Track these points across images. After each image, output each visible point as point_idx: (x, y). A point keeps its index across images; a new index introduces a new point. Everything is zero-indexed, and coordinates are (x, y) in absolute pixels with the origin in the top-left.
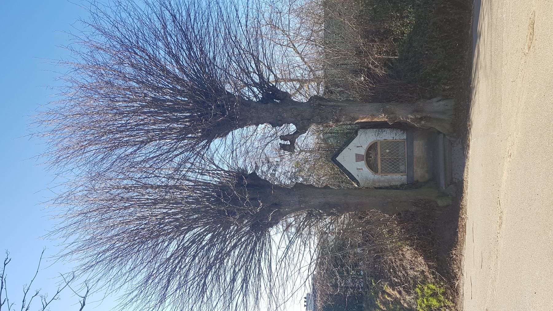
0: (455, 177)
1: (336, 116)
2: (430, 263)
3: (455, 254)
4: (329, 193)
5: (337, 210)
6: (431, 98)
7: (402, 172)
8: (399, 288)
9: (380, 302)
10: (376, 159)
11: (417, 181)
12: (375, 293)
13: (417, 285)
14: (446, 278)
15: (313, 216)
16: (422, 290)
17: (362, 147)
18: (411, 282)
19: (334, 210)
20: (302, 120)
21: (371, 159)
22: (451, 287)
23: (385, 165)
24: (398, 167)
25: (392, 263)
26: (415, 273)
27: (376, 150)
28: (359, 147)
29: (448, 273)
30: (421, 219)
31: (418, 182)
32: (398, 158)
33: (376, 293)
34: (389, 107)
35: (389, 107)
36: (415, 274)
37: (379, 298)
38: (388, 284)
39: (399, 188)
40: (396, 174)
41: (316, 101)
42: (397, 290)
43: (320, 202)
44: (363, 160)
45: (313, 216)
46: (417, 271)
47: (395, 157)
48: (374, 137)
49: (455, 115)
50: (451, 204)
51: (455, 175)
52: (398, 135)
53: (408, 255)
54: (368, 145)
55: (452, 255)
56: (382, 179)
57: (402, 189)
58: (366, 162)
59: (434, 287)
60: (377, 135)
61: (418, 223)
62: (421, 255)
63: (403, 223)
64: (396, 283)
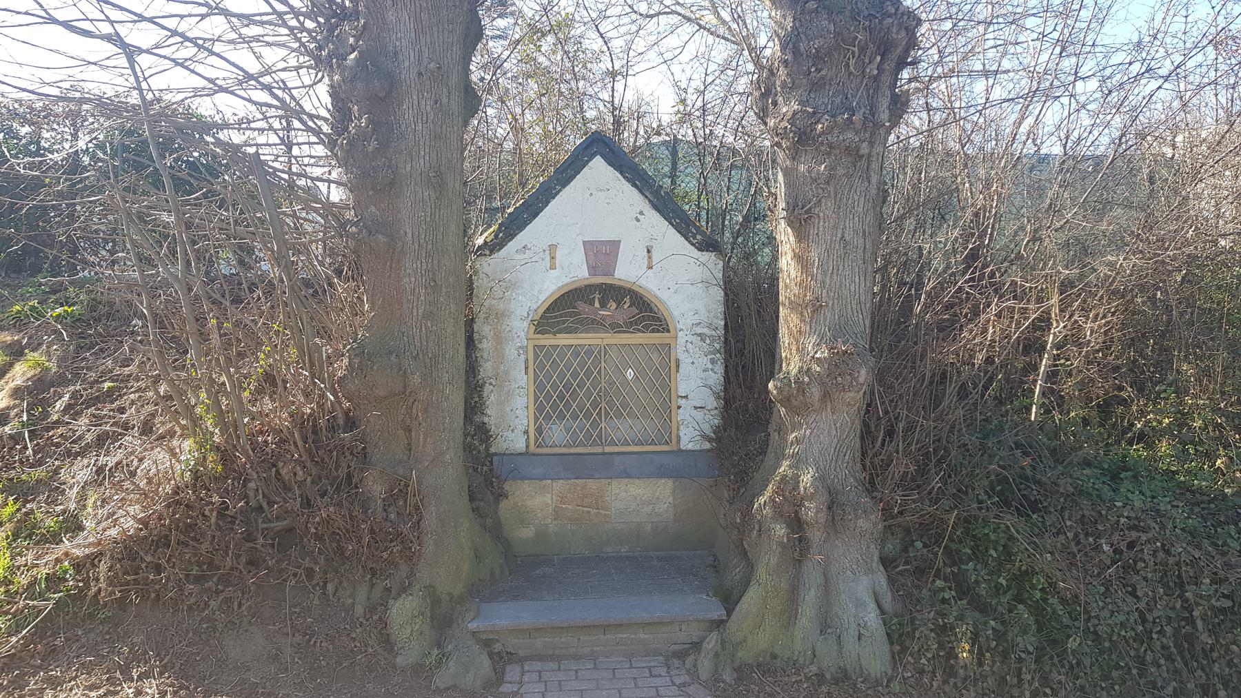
0: (526, 678)
1: (828, 131)
2: (103, 567)
4: (445, 100)
5: (363, 136)
6: (886, 562)
7: (539, 431)
8: (19, 415)
10: (595, 325)
11: (501, 495)
13: (16, 500)
14: (26, 645)
17: (650, 267)
18: (39, 473)
21: (597, 305)
24: (561, 417)
26: (75, 490)
27: (632, 325)
28: (650, 258)
29: (52, 654)
32: (599, 414)
34: (862, 380)
35: (862, 380)
36: (71, 488)
38: (50, 369)
39: (471, 421)
40: (532, 407)
41: (906, 28)
42: (15, 406)
43: (396, 54)
44: (593, 270)
45: (331, 29)
46: (82, 499)
47: (603, 405)
48: (691, 319)
49: (820, 676)
50: (399, 660)
51: (535, 676)
52: (699, 415)
53: (157, 461)
54: (659, 293)
55: (140, 678)
56: (511, 351)
57: (466, 435)
58: (582, 284)
60: (699, 330)
64: (47, 404)
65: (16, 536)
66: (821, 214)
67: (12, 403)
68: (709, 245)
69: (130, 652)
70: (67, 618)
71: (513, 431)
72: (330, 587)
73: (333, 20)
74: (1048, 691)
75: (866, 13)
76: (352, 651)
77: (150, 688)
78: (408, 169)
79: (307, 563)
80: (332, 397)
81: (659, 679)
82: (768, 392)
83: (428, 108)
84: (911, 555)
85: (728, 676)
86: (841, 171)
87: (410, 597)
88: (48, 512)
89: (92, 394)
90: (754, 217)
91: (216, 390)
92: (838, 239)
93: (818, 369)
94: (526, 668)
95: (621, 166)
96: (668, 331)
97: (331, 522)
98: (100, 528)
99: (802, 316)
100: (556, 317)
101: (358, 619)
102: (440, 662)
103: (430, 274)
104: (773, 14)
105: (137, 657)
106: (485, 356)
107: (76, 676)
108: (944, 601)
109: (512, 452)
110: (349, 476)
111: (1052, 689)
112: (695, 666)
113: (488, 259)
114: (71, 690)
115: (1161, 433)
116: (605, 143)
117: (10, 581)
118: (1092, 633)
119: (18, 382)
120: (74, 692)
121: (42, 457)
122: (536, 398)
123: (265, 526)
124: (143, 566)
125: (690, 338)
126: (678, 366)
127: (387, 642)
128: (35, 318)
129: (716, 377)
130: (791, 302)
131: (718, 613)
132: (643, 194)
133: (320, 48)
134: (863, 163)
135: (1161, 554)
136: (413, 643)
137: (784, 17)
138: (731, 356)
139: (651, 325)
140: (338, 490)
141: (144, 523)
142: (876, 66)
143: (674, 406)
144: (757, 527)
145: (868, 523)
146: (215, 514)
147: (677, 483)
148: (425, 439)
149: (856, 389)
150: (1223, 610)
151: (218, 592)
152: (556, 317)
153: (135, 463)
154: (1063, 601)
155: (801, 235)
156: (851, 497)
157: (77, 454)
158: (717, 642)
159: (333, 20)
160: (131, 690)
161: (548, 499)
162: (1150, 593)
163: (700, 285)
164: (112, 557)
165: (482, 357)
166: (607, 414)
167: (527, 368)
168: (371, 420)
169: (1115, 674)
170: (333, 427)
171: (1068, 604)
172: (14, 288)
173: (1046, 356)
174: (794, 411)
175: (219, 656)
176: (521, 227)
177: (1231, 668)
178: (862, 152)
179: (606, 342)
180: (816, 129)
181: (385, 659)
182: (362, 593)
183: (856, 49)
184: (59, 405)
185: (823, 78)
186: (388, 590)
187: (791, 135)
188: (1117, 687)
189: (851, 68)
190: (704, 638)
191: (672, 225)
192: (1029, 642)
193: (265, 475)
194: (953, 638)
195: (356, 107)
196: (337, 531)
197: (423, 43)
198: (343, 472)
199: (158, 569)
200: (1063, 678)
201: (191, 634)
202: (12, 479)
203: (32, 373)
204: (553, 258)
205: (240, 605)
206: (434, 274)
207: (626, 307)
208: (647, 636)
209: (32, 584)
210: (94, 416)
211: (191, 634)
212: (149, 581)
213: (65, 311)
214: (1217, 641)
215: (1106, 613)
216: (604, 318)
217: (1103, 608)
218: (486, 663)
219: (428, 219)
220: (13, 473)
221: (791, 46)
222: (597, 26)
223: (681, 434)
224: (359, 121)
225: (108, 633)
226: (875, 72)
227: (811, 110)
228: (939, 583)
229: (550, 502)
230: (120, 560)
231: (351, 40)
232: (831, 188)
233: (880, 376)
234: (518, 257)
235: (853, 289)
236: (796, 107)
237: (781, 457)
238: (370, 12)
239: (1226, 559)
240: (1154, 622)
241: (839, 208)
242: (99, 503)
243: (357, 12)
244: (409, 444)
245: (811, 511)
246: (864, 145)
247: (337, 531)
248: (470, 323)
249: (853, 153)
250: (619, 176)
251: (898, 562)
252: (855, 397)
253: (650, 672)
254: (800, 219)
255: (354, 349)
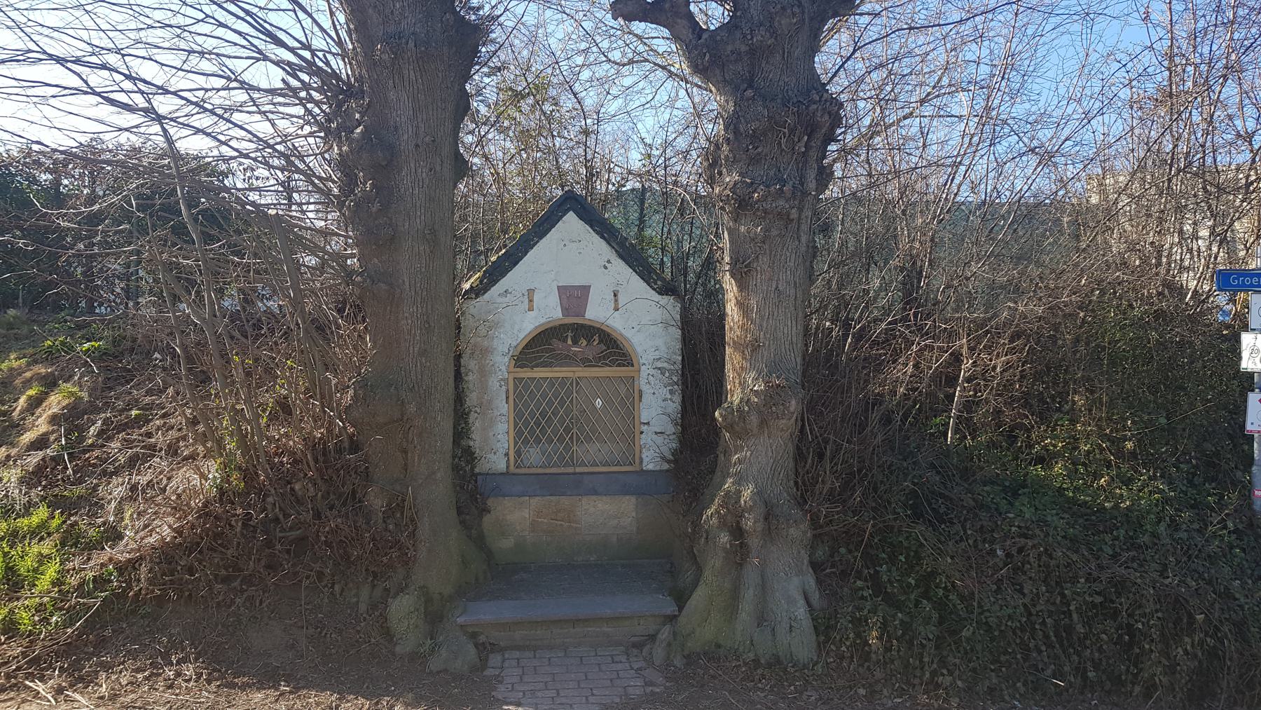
0: (506, 664)
1: (763, 199)
2: (144, 569)
3: (178, 674)
4: (438, 168)
5: (368, 198)
6: (816, 566)
7: (518, 453)
8: (58, 439)
9: (11, 369)
10: (569, 360)
12: (49, 352)
13: (62, 513)
14: (79, 636)
15: (339, 105)
16: (38, 533)
17: (616, 309)
18: (79, 490)
19: (364, 184)
20: (752, 51)
21: (570, 342)
22: (35, 661)
23: (544, 396)
24: (538, 441)
25: (164, 416)
26: (113, 505)
27: (600, 360)
28: (616, 301)
29: (101, 644)
30: (332, 529)
31: (484, 510)
32: (571, 438)
33: (50, 356)
34: (792, 409)
35: (792, 409)
36: (109, 503)
37: (29, 364)
41: (829, 113)
42: (53, 431)
43: (396, 128)
44: (566, 311)
45: (339, 105)
46: (119, 512)
47: (575, 430)
48: (652, 355)
49: (756, 661)
50: (398, 649)
51: (514, 663)
52: (659, 440)
53: (185, 478)
54: (623, 332)
55: (178, 663)
56: (494, 383)
57: (454, 457)
58: (557, 324)
59: (44, 582)
60: (659, 365)
61: (319, 518)
62: (179, 532)
63: (316, 461)
64: (82, 430)
65: (63, 544)
66: (759, 268)
67: (51, 429)
68: (666, 289)
69: (168, 642)
70: (112, 614)
71: (495, 453)
72: (337, 587)
73: (341, 97)
74: (945, 672)
75: (795, 100)
76: (357, 641)
77: (188, 671)
78: (407, 227)
79: (317, 567)
80: (341, 424)
81: (620, 664)
82: (714, 419)
83: (424, 174)
84: (837, 559)
85: (678, 662)
86: (774, 232)
87: (407, 596)
88: (90, 524)
89: (122, 420)
90: (710, 264)
91: (237, 415)
92: (773, 289)
93: (756, 400)
94: (507, 656)
95: (591, 220)
96: (632, 365)
97: (339, 531)
98: (138, 537)
99: (744, 354)
100: (533, 353)
101: (362, 615)
102: (433, 650)
103: (425, 317)
104: (718, 98)
105: (175, 645)
106: (471, 386)
107: (124, 661)
108: (863, 598)
109: (495, 472)
110: (354, 492)
111: (948, 670)
112: (651, 653)
113: (474, 302)
114: (121, 672)
115: (1055, 456)
116: (576, 200)
117: (61, 583)
118: (985, 624)
119: (55, 410)
120: (123, 674)
121: (80, 477)
122: (516, 425)
123: (281, 535)
124: (179, 568)
125: (652, 372)
126: (641, 397)
127: (388, 634)
128: (65, 352)
129: (674, 406)
130: (734, 342)
131: (671, 609)
132: (610, 245)
133: (329, 121)
134: (794, 224)
135: (1044, 558)
136: (410, 634)
137: (727, 101)
138: (687, 387)
139: (617, 360)
140: (344, 504)
141: (179, 532)
142: (803, 144)
143: (637, 433)
144: (704, 535)
145: (799, 531)
146: (240, 524)
147: (640, 500)
148: (420, 459)
149: (787, 417)
150: (1094, 605)
151: (242, 591)
152: (533, 353)
153: (165, 481)
154: (962, 598)
155: (742, 286)
156: (785, 509)
157: (112, 474)
158: (669, 633)
159: (341, 97)
160: (172, 673)
161: (526, 514)
162: (1034, 590)
163: (660, 325)
164: (151, 561)
165: (468, 388)
166: (578, 439)
167: (507, 398)
168: (373, 443)
169: (1003, 658)
170: (340, 449)
171: (967, 601)
172: (42, 324)
173: (959, 389)
174: (737, 435)
175: (245, 645)
176: (503, 273)
177: (1101, 654)
178: (791, 217)
179: (577, 375)
180: (753, 197)
181: (386, 648)
182: (365, 592)
183: (786, 130)
184: (93, 430)
185: (759, 154)
186: (386, 590)
187: (733, 202)
188: (1004, 669)
189: (783, 146)
190: (659, 631)
191: (636, 272)
192: (931, 631)
193: (281, 491)
194: (867, 628)
195: (361, 174)
196: (344, 539)
197: (420, 120)
198: (347, 489)
199: (191, 571)
200: (957, 661)
201: (220, 627)
202: (57, 495)
203: (67, 402)
204: (531, 301)
205: (261, 603)
206: (428, 317)
207: (595, 343)
208: (610, 629)
209: (81, 585)
210: (125, 440)
211: (220, 627)
212: (184, 580)
213: (92, 346)
214: (1091, 631)
215: (997, 607)
216: (575, 354)
217: (994, 602)
218: (472, 651)
219: (423, 270)
220: (56, 490)
221: (732, 127)
222: (570, 87)
223: (644, 456)
224: (364, 185)
225: (148, 626)
226: (803, 149)
227: (749, 181)
228: (859, 583)
229: (527, 516)
230: (158, 564)
231: (357, 116)
232: (766, 247)
233: (811, 407)
234: (500, 300)
235: (786, 332)
236: (737, 178)
237: (726, 475)
238: (374, 92)
239: (1099, 562)
240: (1037, 615)
241: (774, 264)
242: (135, 516)
243: (363, 92)
244: (406, 464)
245: (749, 523)
246: (794, 211)
247: (344, 539)
248: (458, 357)
249: (785, 217)
250: (590, 229)
251: (825, 565)
252: (787, 424)
253: (612, 658)
254: (742, 272)
255: (359, 382)
